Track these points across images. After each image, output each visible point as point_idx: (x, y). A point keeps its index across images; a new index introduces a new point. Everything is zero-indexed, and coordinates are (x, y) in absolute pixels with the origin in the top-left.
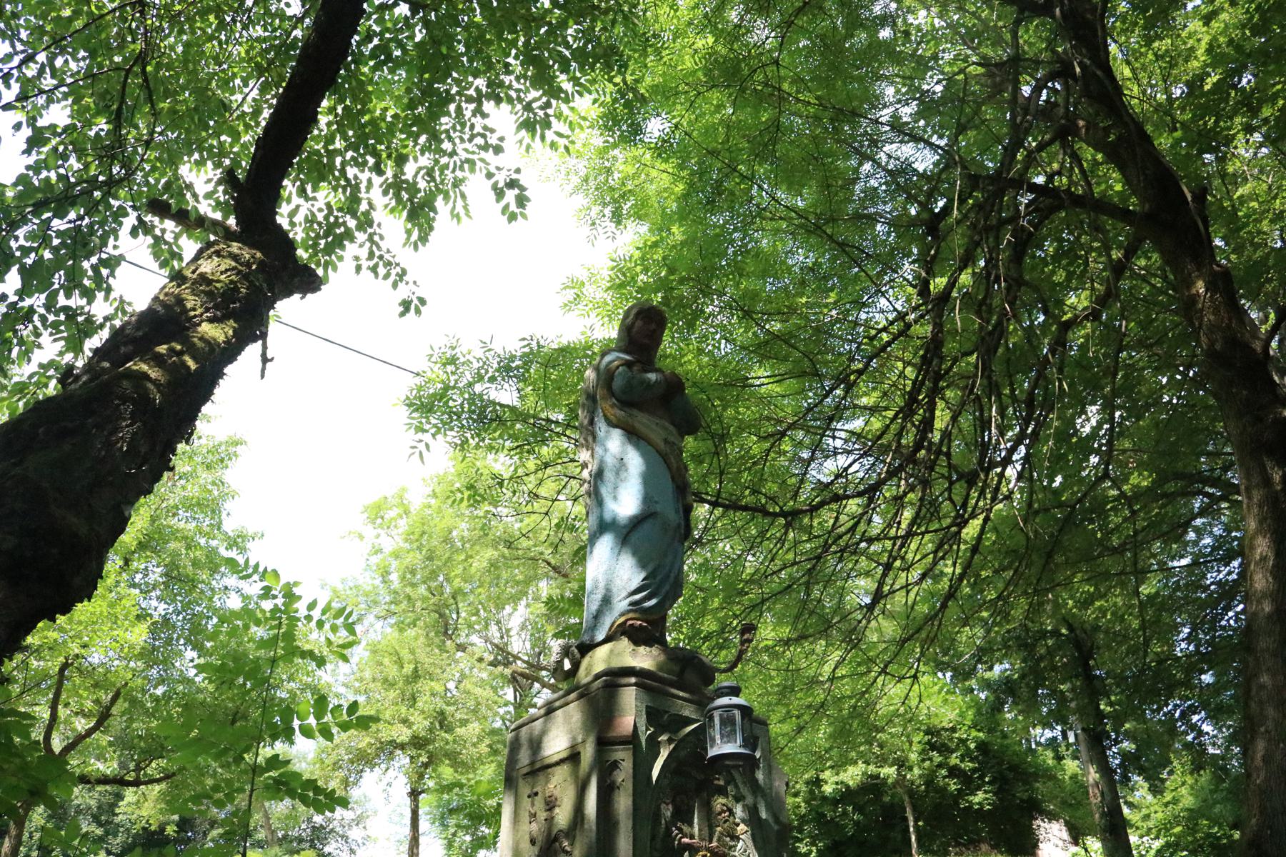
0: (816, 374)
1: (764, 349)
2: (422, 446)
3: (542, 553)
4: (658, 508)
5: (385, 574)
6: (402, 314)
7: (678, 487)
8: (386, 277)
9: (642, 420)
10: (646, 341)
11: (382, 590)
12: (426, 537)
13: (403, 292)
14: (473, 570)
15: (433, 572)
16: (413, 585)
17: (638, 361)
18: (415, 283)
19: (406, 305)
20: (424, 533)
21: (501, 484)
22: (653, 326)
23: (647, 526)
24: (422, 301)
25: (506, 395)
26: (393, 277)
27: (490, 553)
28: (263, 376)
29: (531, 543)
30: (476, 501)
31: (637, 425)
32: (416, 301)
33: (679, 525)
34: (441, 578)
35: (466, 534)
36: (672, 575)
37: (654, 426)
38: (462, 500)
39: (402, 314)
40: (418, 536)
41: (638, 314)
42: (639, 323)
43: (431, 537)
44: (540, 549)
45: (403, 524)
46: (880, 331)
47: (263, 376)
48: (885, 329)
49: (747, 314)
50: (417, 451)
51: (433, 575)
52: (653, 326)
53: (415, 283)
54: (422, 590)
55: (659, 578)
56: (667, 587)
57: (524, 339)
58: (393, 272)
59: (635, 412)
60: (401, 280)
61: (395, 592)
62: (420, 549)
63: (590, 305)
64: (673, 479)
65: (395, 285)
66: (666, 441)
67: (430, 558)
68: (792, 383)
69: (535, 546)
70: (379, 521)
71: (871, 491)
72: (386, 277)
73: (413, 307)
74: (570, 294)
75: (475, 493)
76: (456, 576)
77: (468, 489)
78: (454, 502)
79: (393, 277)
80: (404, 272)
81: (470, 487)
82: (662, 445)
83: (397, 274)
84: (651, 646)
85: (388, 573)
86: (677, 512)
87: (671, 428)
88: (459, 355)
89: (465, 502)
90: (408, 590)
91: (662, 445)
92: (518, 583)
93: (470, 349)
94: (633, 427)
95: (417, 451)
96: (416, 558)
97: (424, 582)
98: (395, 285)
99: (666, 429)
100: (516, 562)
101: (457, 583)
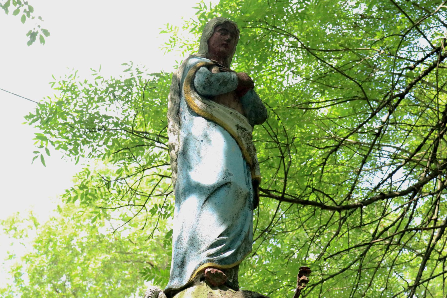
0: (366, 99)
1: (323, 81)
2: (43, 151)
3: (146, 256)
4: (232, 179)
5: (17, 276)
6: (30, 43)
7: (248, 164)
8: (16, 12)
9: (219, 110)
10: (222, 49)
11: (16, 288)
12: (51, 244)
13: (31, 25)
14: (90, 271)
15: (58, 273)
16: (41, 284)
17: (217, 65)
18: (40, 18)
19: (33, 35)
20: (50, 240)
21: (108, 184)
22: (228, 37)
23: (222, 193)
24: (46, 33)
25: (115, 111)
26: (21, 13)
27: (104, 257)
28: (45, 166)
29: (138, 248)
30: (87, 199)
31: (214, 114)
32: (41, 33)
33: (249, 194)
34: (64, 278)
35: (85, 241)
36: (243, 234)
37: (229, 115)
38: (76, 198)
39: (30, 43)
40: (46, 242)
41: (216, 27)
42: (218, 34)
43: (55, 244)
44: (146, 253)
45: (34, 234)
46: (418, 62)
47: (45, 166)
48: (422, 61)
49: (310, 52)
50: (39, 155)
51: (58, 274)
52: (228, 37)
53: (40, 18)
54: (49, 288)
55: (232, 235)
56: (239, 243)
57: (125, 64)
58: (22, 9)
59: (213, 103)
60: (29, 15)
61: (26, 289)
62: (46, 253)
63: (185, 47)
64: (244, 158)
65: (23, 19)
66: (238, 127)
67: (55, 262)
68: (346, 107)
69: (140, 250)
70: (13, 231)
71: (416, 190)
72: (16, 12)
73: (38, 38)
74: (167, 37)
75: (86, 195)
76: (76, 275)
77: (81, 188)
78: (69, 199)
79: (21, 13)
80: (31, 9)
81: (82, 187)
82: (234, 130)
83: (25, 11)
84: (225, 290)
85: (20, 274)
86: (247, 183)
87: (243, 117)
88: (77, 84)
89: (78, 201)
90: (37, 287)
91: (234, 130)
92: (126, 281)
93: (84, 79)
94: (212, 115)
95: (39, 155)
96: (44, 261)
97: (50, 282)
98: (23, 19)
99: (239, 118)
100: (126, 264)
101: (77, 281)
